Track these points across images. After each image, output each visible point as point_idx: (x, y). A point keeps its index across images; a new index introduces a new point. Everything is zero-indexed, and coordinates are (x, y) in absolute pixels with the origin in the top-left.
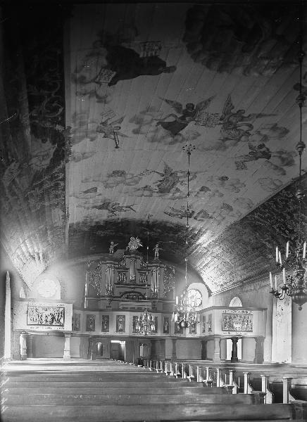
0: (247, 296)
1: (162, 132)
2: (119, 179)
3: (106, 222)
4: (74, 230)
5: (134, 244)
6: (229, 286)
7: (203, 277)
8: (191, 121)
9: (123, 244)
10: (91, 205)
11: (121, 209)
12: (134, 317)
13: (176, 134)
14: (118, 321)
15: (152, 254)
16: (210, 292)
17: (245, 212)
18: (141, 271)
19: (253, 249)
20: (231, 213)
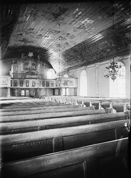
0: (71, 74)
1: (52, 16)
2: (81, 31)
3: (22, 46)
4: (9, 49)
5: (31, 55)
6: (63, 70)
7: (53, 66)
8: (63, 14)
9: (26, 54)
10: (18, 40)
11: (29, 42)
12: (60, 85)
13: (56, 18)
14: (26, 83)
15: (37, 59)
16: (56, 72)
17: (73, 46)
18: (33, 64)
19: (74, 58)
20: (68, 46)
